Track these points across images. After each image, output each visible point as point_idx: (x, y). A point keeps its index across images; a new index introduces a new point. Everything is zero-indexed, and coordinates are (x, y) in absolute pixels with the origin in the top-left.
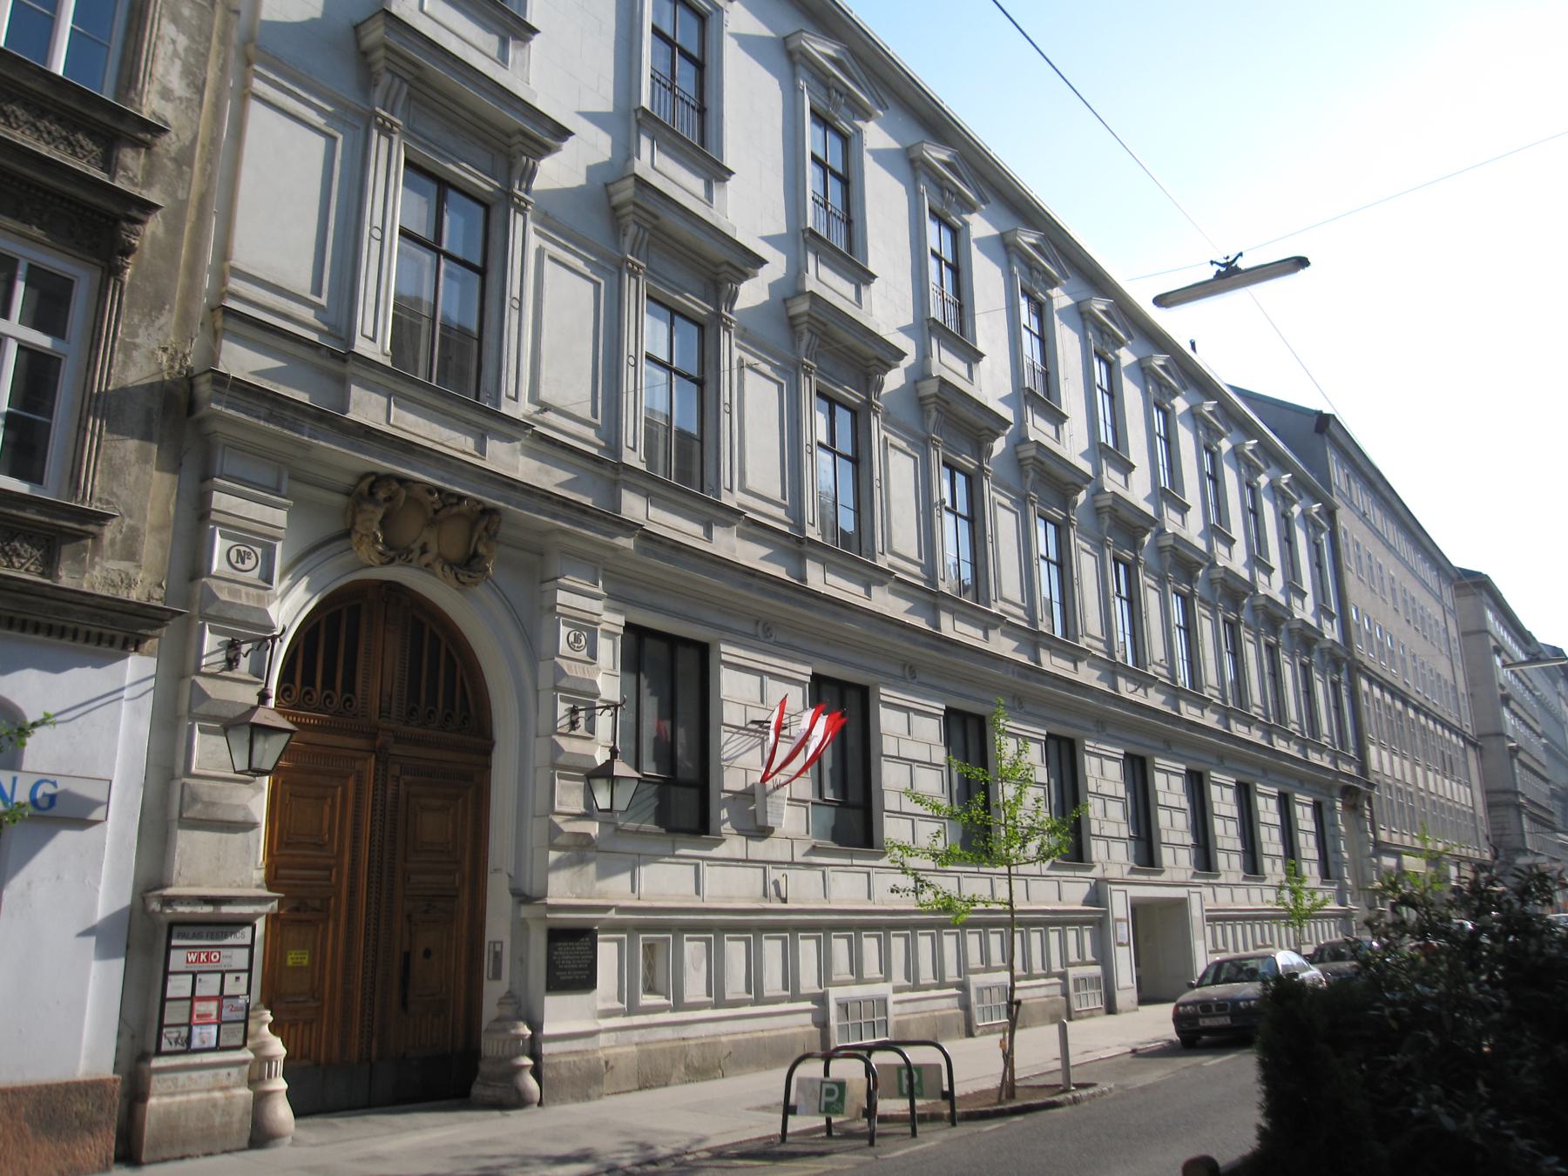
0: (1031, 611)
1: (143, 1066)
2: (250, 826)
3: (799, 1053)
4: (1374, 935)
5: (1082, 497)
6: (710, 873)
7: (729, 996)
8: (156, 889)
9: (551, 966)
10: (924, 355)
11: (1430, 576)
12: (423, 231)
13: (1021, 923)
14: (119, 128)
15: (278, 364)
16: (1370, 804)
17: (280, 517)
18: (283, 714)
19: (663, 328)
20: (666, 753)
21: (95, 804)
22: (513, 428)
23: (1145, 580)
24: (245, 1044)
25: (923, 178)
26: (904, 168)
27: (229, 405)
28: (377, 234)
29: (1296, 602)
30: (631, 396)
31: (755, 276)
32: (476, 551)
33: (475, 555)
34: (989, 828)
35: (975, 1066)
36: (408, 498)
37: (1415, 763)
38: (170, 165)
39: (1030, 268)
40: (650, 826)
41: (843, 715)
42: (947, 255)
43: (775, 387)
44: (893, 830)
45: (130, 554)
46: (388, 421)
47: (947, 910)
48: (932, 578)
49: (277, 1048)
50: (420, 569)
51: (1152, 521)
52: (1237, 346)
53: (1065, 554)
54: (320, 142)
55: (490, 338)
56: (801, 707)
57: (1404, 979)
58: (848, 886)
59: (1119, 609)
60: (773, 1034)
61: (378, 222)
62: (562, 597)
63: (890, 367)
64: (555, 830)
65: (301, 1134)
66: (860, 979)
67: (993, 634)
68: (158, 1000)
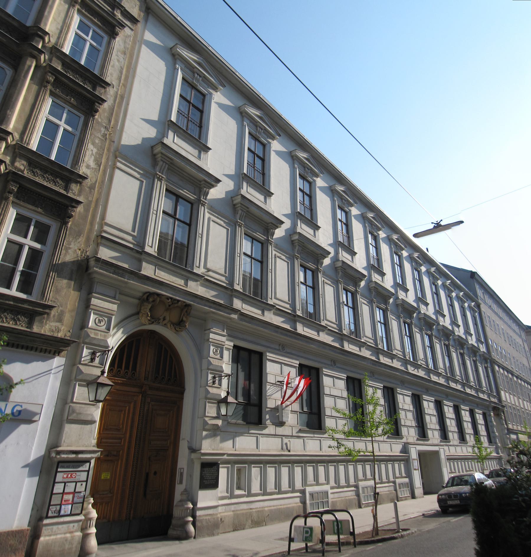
0: (375, 341)
1: (40, 523)
2: (93, 422)
3: (295, 515)
4: (511, 467)
5: (391, 300)
6: (262, 440)
7: (268, 491)
8: (54, 448)
9: (202, 478)
10: (337, 253)
11: (516, 328)
12: (170, 211)
13: (378, 460)
14: (71, 177)
15: (158, 42)
16: (504, 414)
17: (115, 307)
18: (109, 379)
19: (249, 244)
20: (247, 393)
21: (35, 414)
22: (197, 277)
23: (415, 330)
24: (81, 513)
25: (336, 196)
26: (329, 193)
27: (100, 268)
28: (155, 212)
29: (469, 338)
30: (238, 266)
31: (280, 227)
32: (182, 319)
33: (182, 321)
34: (364, 422)
35: (362, 521)
36: (160, 301)
37: (519, 398)
38: (87, 189)
39: (372, 225)
40: (240, 422)
41: (310, 379)
42: (344, 220)
43: (286, 264)
44: (329, 423)
45: (60, 320)
46: (155, 274)
47: (350, 455)
48: (340, 329)
49: (94, 514)
50: (163, 326)
51: (416, 309)
52: (442, 250)
53: (387, 321)
54: (138, 182)
55: (191, 247)
56: (295, 376)
57: (525, 485)
58: (312, 445)
59: (407, 340)
60: (285, 506)
61: (155, 208)
62: (212, 336)
63: (325, 257)
64: (206, 423)
65: (100, 552)
66: (318, 484)
67: (362, 349)
68: (52, 483)
